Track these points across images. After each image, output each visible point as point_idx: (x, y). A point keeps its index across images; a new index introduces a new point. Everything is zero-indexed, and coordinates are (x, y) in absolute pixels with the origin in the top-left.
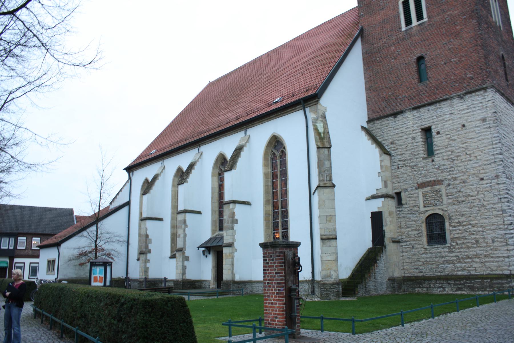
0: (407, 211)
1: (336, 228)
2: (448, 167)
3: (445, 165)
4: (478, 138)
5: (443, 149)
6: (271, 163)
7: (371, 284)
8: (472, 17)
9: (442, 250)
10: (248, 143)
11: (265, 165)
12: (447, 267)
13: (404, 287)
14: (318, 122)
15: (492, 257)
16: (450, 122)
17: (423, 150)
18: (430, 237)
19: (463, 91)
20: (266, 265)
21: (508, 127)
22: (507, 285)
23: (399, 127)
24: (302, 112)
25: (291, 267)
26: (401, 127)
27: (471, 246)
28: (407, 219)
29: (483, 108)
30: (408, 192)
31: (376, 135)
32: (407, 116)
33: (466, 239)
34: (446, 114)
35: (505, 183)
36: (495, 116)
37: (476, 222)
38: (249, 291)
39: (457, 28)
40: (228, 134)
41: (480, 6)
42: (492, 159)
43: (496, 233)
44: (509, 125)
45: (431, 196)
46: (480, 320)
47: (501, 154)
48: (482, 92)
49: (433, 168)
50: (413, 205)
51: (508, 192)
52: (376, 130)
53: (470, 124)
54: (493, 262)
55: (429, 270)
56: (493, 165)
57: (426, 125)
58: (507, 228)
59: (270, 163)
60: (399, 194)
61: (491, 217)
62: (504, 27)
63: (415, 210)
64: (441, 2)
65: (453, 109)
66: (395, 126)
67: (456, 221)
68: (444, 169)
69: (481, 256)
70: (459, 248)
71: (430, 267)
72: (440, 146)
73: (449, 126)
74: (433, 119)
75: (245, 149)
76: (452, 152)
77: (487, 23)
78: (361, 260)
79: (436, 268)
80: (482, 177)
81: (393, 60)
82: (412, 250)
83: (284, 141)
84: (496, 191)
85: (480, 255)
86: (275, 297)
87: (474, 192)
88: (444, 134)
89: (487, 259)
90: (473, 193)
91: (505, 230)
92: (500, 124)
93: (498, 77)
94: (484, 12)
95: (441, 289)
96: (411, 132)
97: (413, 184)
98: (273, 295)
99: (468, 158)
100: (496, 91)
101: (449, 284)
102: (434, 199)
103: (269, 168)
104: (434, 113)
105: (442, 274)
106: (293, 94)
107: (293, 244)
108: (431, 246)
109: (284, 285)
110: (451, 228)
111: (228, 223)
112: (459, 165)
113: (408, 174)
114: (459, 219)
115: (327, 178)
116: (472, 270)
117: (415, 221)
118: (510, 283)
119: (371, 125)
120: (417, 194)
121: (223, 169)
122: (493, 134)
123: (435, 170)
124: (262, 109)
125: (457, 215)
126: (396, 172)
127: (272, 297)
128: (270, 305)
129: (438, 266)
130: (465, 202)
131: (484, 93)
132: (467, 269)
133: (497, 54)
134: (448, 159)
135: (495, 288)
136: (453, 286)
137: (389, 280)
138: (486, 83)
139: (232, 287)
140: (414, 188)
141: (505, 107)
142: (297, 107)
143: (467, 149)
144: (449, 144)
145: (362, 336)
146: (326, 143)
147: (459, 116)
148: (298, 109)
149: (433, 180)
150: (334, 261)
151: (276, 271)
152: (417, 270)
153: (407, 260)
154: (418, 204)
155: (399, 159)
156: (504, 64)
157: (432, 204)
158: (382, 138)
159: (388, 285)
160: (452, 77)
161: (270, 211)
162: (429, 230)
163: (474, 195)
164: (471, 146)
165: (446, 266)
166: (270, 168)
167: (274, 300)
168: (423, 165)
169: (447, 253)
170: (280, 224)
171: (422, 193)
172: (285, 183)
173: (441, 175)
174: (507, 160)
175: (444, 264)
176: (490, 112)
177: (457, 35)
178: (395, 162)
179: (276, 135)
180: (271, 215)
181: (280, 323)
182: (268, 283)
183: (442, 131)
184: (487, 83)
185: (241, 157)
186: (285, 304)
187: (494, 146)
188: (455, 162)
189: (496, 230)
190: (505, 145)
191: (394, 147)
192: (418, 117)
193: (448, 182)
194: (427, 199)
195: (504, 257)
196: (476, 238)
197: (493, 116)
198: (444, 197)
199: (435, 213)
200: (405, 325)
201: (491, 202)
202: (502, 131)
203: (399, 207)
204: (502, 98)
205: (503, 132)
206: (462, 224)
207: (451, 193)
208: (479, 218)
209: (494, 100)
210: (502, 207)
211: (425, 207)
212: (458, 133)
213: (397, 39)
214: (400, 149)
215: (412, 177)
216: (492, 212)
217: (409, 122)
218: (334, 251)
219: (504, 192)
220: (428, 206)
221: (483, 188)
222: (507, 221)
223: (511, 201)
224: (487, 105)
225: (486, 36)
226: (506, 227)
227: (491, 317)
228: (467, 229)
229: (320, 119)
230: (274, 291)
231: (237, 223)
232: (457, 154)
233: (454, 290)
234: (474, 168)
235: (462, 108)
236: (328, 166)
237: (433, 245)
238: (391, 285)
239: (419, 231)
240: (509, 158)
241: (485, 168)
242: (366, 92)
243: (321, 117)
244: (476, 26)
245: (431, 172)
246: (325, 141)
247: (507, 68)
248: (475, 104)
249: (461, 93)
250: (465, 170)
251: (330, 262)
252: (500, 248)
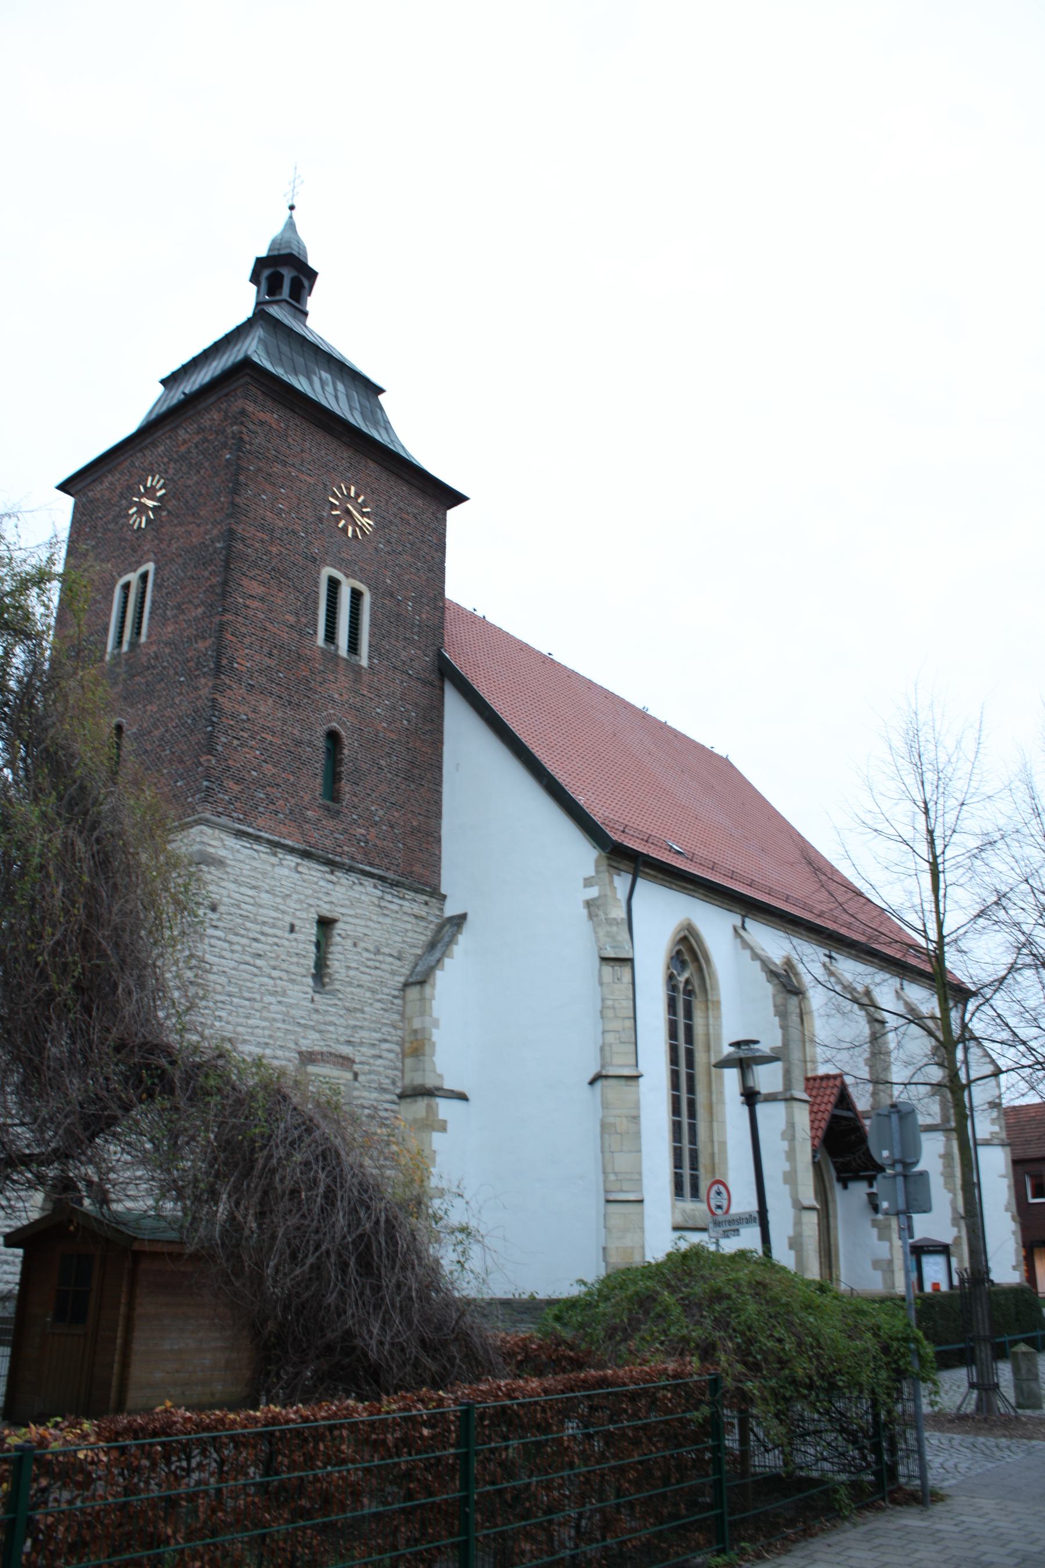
57: (326, 911)
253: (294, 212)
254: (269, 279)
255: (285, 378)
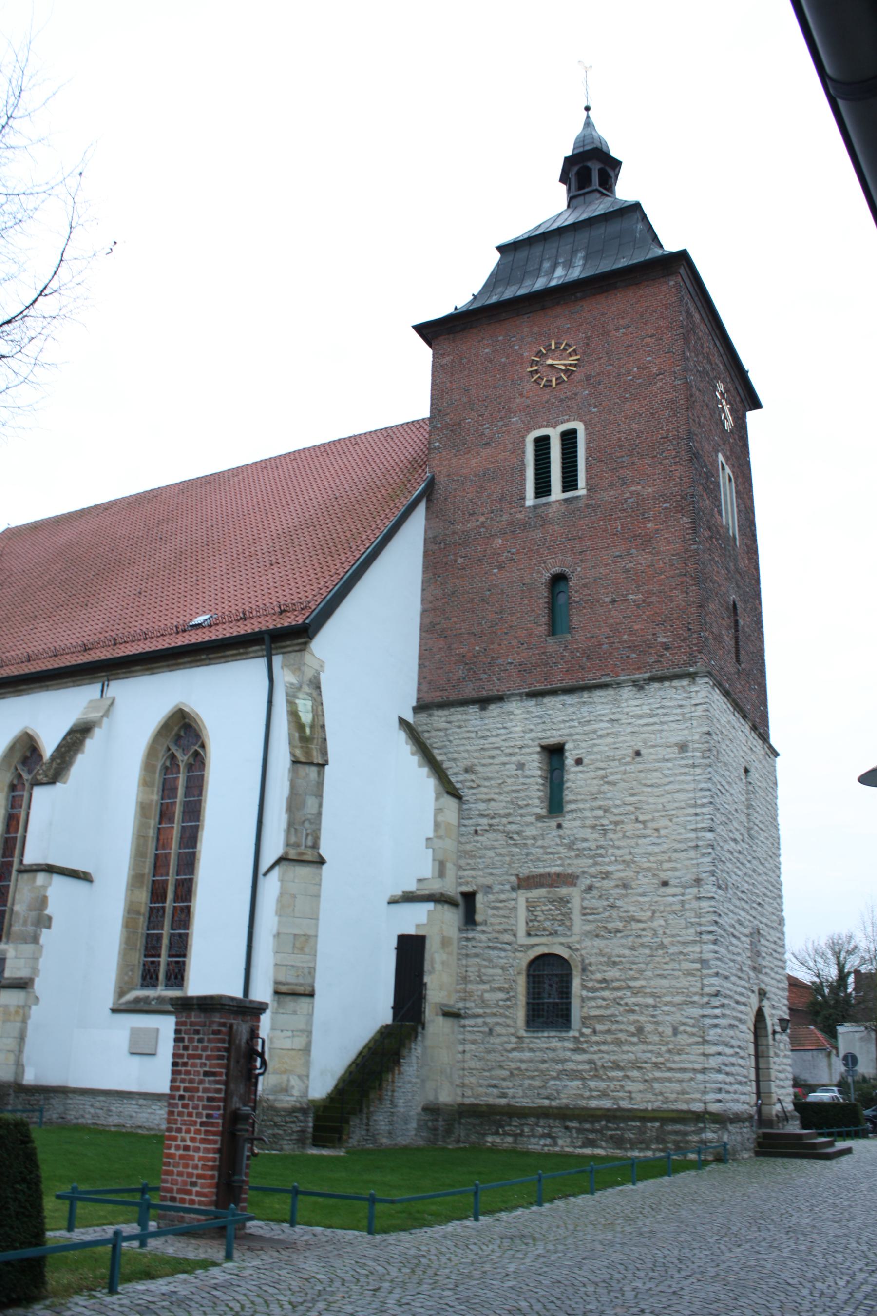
0: (486, 942)
1: (314, 968)
2: (594, 847)
3: (585, 840)
4: (667, 788)
5: (586, 801)
6: (162, 780)
7: (381, 1118)
8: (683, 509)
9: (559, 1044)
10: (107, 717)
11: (145, 783)
12: (566, 1086)
13: (460, 1131)
14: (301, 695)
15: (670, 1070)
16: (609, 740)
17: (539, 798)
18: (533, 1010)
19: (645, 672)
20: (181, 1052)
21: (731, 768)
22: (695, 1138)
23: (488, 733)
24: (262, 663)
25: (242, 1061)
26: (494, 733)
27: (626, 1040)
28: (484, 960)
29: (683, 719)
30: (493, 894)
31: (431, 745)
32: (511, 709)
33: (617, 1022)
34: (602, 721)
35: (713, 898)
36: (707, 742)
37: (643, 983)
38: (55, 1116)
39: (649, 526)
40: (52, 685)
41: (701, 487)
42: (692, 841)
43: (683, 1013)
44: (734, 764)
45: (547, 911)
46: (641, 1213)
47: (711, 830)
48: (685, 682)
49: (557, 845)
50: (500, 927)
51: (716, 918)
52: (434, 733)
53: (652, 750)
54: (670, 1080)
55: (523, 1090)
56: (692, 854)
57: (553, 739)
58: (708, 1003)
59: (157, 778)
60: (469, 898)
61: (676, 973)
62: (741, 540)
63: (506, 941)
64: (620, 460)
65: (619, 710)
66: (480, 730)
67: (599, 976)
68: (584, 849)
69: (644, 1065)
70: (598, 1043)
71: (526, 1085)
72: (580, 795)
73: (606, 748)
74: (570, 727)
75: (97, 732)
76: (606, 811)
77: (710, 529)
78: (360, 1053)
79: (540, 1088)
80: (665, 878)
81: (495, 571)
82: (487, 1039)
83: (205, 727)
84: (693, 915)
85: (642, 1063)
86: (197, 1132)
87: (644, 911)
88: (591, 766)
89: (658, 1074)
90: (642, 914)
91: (703, 1006)
92: (715, 760)
93: (721, 652)
94: (707, 502)
95: (548, 1141)
96: (517, 750)
97: (506, 877)
98: (192, 1128)
99: (639, 829)
100: (714, 685)
101: (567, 1128)
102: (553, 920)
103: (155, 792)
104: (574, 713)
105: (554, 1104)
106: (244, 614)
107: (251, 1006)
108: (534, 1032)
109: (221, 1104)
110: (584, 993)
111: (25, 923)
112: (617, 843)
113: (497, 850)
114: (605, 971)
115: (306, 838)
116: (622, 1099)
117: (503, 968)
118: (701, 1133)
119: (423, 717)
120: (513, 902)
121: (25, 776)
122: (699, 781)
123: (561, 849)
124: (158, 637)
125: (601, 963)
126: (470, 842)
127: (188, 1131)
128: (181, 1152)
129: (546, 1083)
130: (622, 934)
131: (689, 685)
132: (611, 1093)
133: (724, 600)
134: (593, 827)
135: (669, 1143)
136: (575, 1135)
137: (425, 1109)
138: (695, 663)
139: (11, 1102)
140: (508, 887)
141: (729, 722)
142: (251, 649)
143: (640, 808)
144: (600, 792)
145: (392, 1238)
146: (315, 753)
147: (629, 729)
148: (252, 655)
149: (555, 874)
150: (300, 1052)
151: (207, 1069)
152: (495, 1091)
153: (472, 1064)
154: (514, 928)
155: (479, 810)
156: (736, 622)
157: (547, 930)
158: (446, 754)
159: (422, 1123)
160: (625, 637)
161: (143, 906)
162: (534, 993)
163: (644, 918)
164: (648, 804)
165: (564, 1083)
166: (158, 791)
167: (193, 1140)
168: (535, 833)
169: (568, 1053)
170: (165, 941)
171: (527, 901)
172: (191, 838)
173: (575, 862)
174: (722, 844)
175: (560, 1080)
176: (698, 730)
177: (646, 541)
178: (471, 818)
179: (186, 709)
180: (144, 915)
181: (203, 1199)
182: (182, 1097)
183: (589, 757)
184: (699, 664)
185: (83, 752)
186: (219, 1151)
187: (698, 810)
188: (611, 835)
189: (684, 1006)
190: (722, 810)
191: (473, 781)
192: (537, 717)
193: (588, 882)
194: (536, 916)
195: (694, 1070)
196: (638, 1021)
197: (703, 740)
198: (576, 917)
199: (551, 952)
200: (481, 1218)
201: (679, 938)
202: (718, 778)
203: (467, 930)
204: (726, 700)
205: (720, 779)
206: (611, 986)
207: (593, 909)
208: (649, 974)
209: (708, 705)
210: (701, 953)
211: (529, 935)
212: (623, 768)
213: (510, 523)
214: (485, 787)
215: (507, 859)
216: (680, 964)
217: (514, 724)
218: (302, 1026)
219: (709, 919)
220: (537, 935)
221: (665, 905)
222: (709, 986)
223: (722, 940)
224: (693, 714)
225: (707, 556)
226: (706, 999)
227: (662, 1208)
228: (621, 998)
229: (306, 689)
230: (194, 1118)
231: (49, 927)
232: (617, 818)
233: (577, 1145)
234: (650, 854)
235: (638, 711)
236: (314, 811)
237: (538, 1031)
238: (430, 1124)
239: (508, 993)
240: (726, 841)
241: (673, 858)
242: (421, 635)
243: (308, 685)
244: (688, 532)
245: (551, 853)
246: (313, 746)
247: (740, 633)
248: (669, 707)
249: (641, 676)
250: (631, 857)
251: (291, 1052)
252: (688, 1049)
253: (590, 112)
254: (578, 174)
255: (522, 292)
